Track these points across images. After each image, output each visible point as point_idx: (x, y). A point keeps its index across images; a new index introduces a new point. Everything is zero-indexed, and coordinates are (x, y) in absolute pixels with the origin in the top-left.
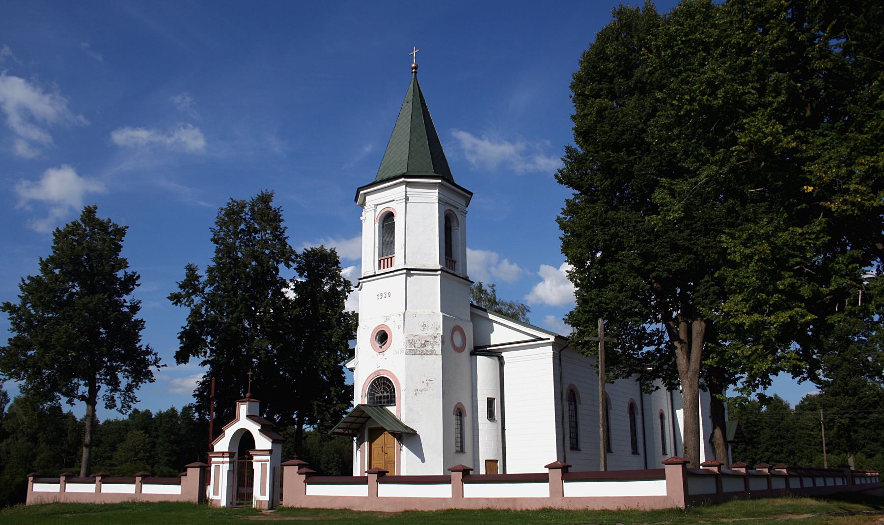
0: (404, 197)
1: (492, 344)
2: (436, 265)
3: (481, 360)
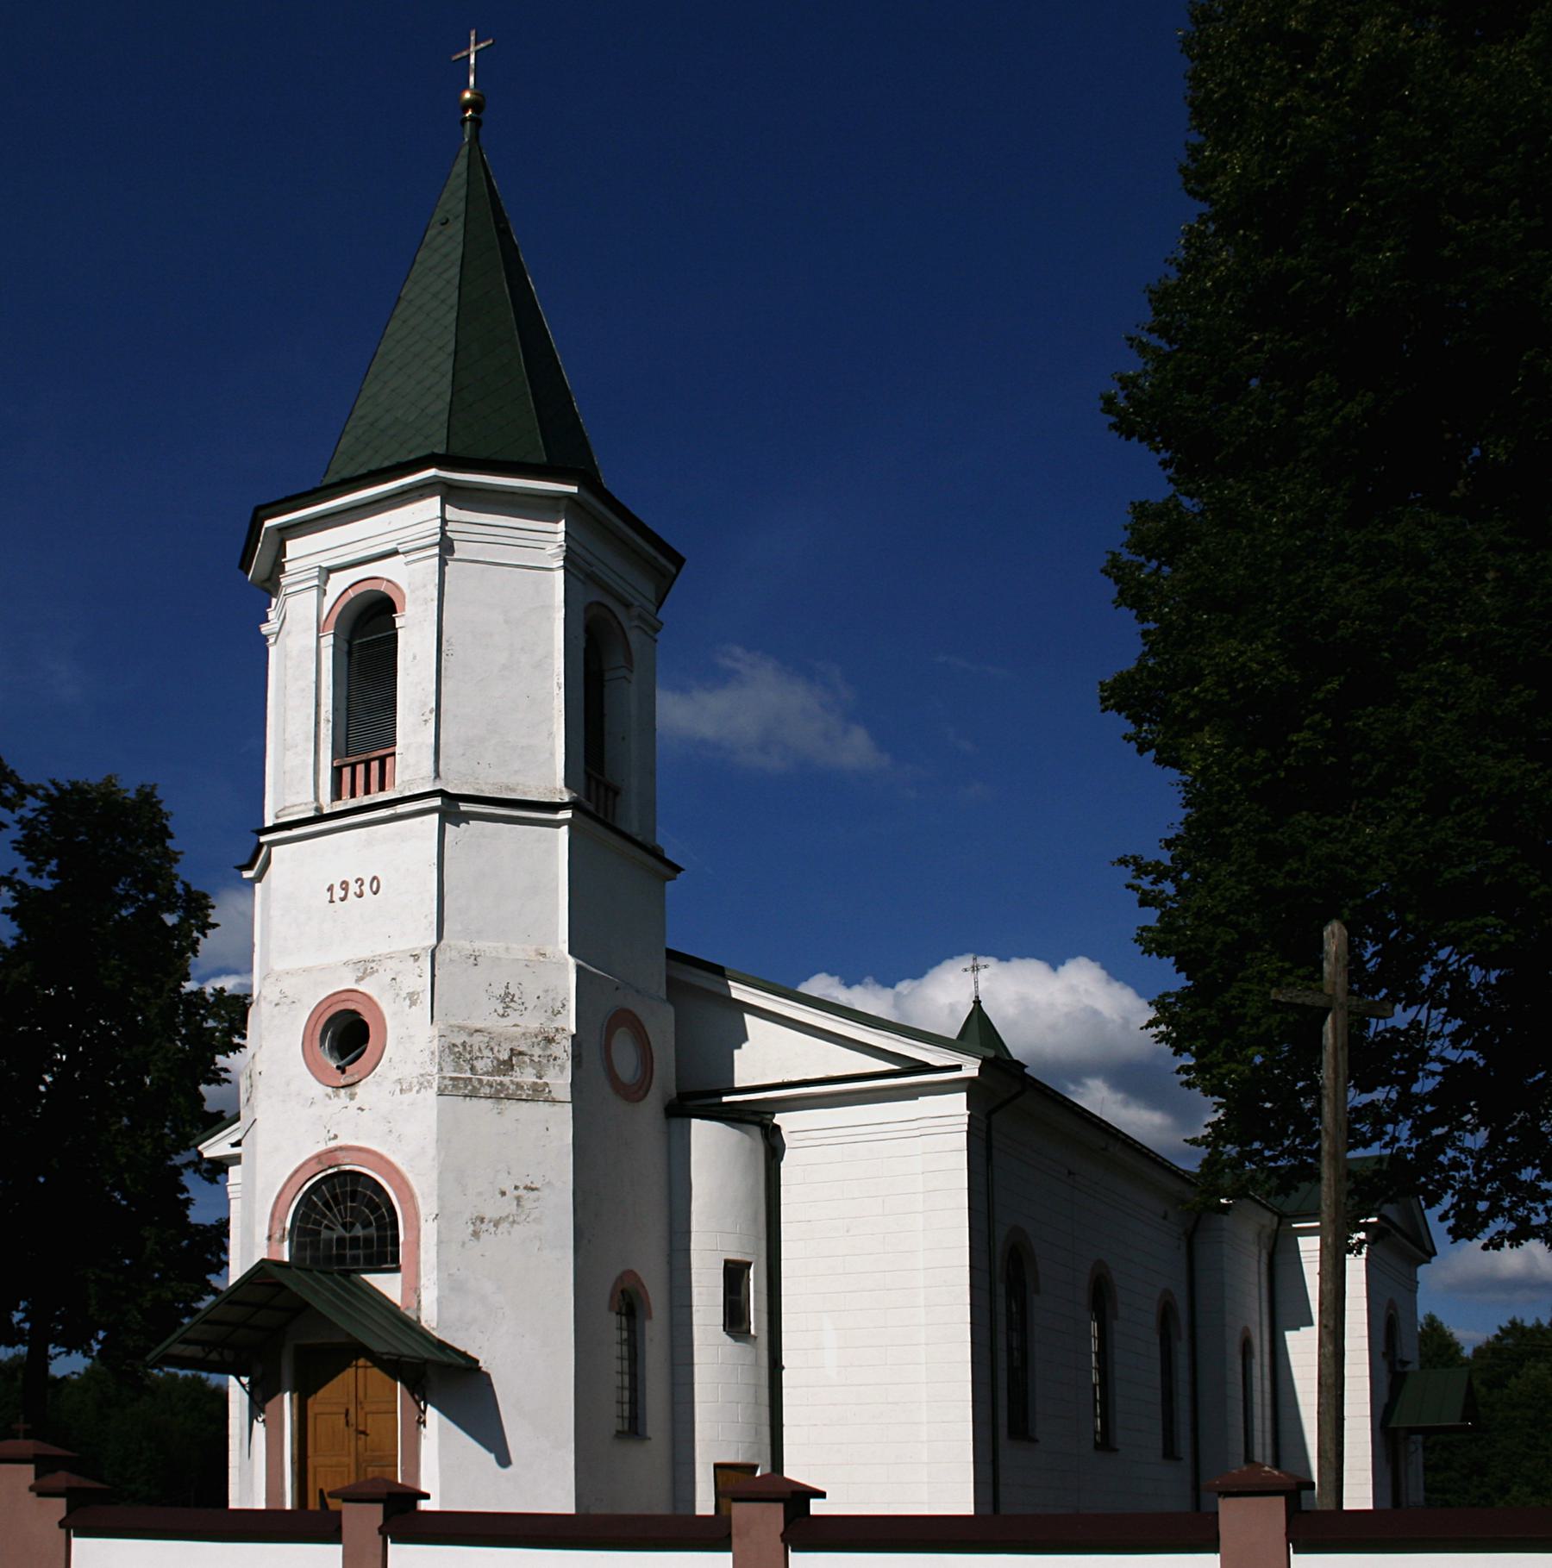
0: (437, 538)
1: (738, 1084)
2: (553, 791)
3: (705, 1136)
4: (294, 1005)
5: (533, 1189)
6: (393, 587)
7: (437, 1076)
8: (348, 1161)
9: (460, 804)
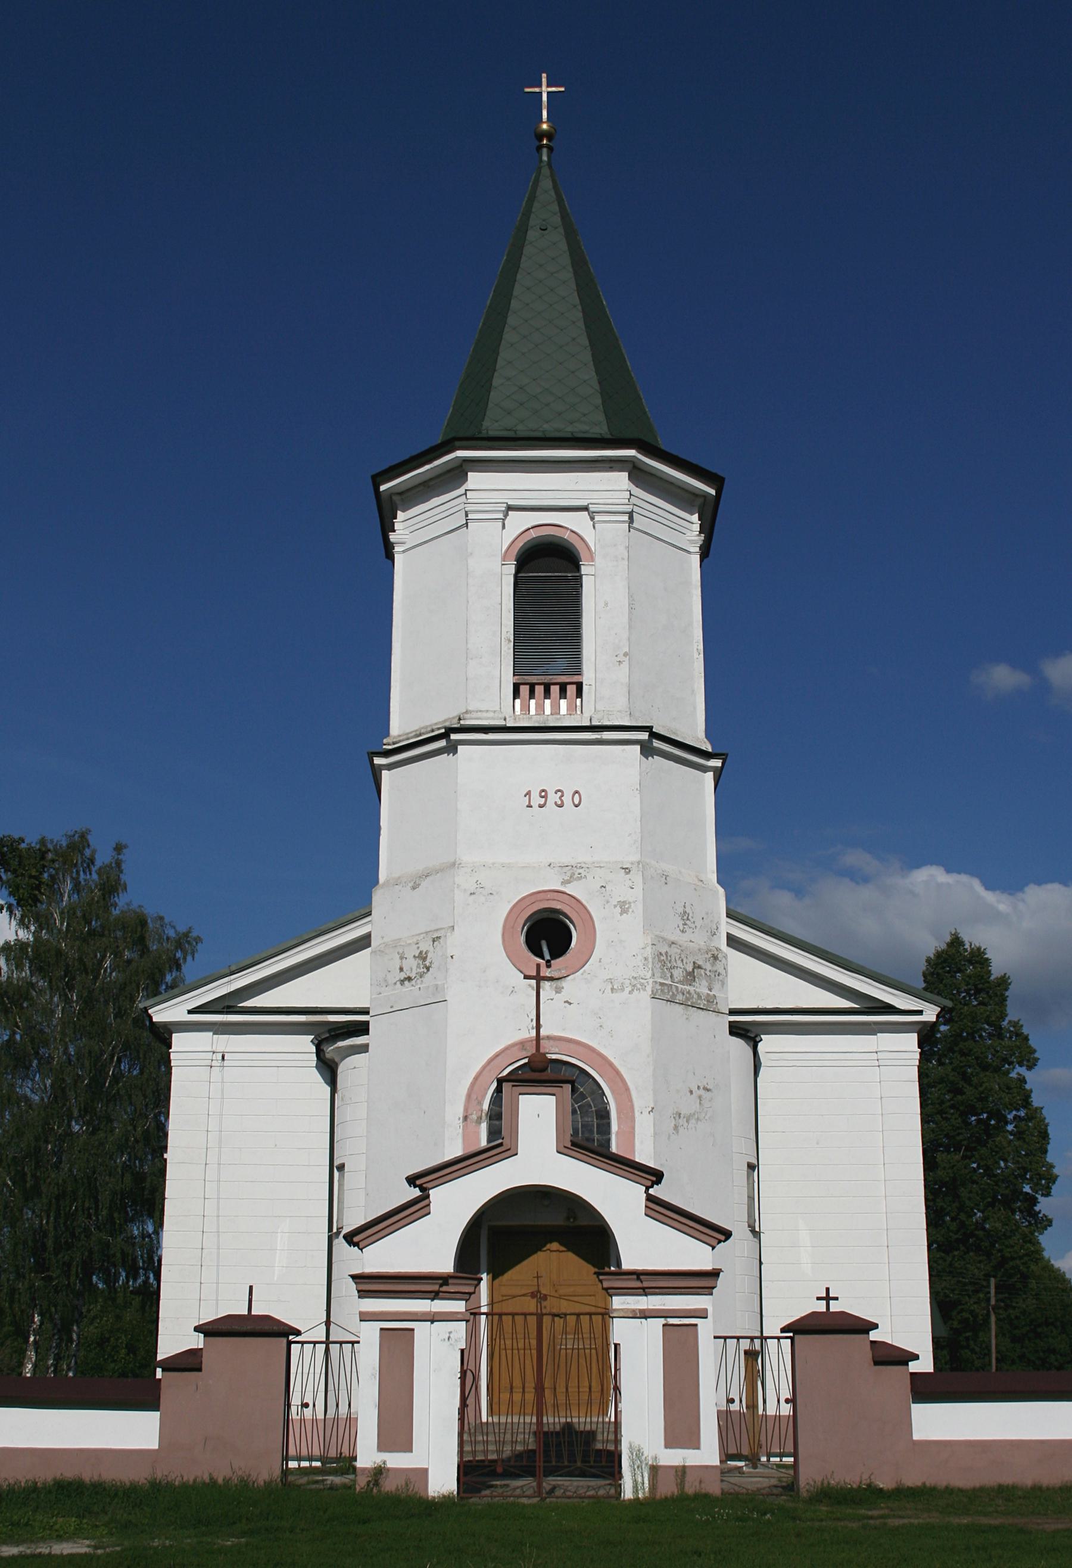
4: (492, 896)
5: (708, 1090)
6: (578, 538)
7: (651, 981)
8: (557, 1050)
9: (654, 740)
